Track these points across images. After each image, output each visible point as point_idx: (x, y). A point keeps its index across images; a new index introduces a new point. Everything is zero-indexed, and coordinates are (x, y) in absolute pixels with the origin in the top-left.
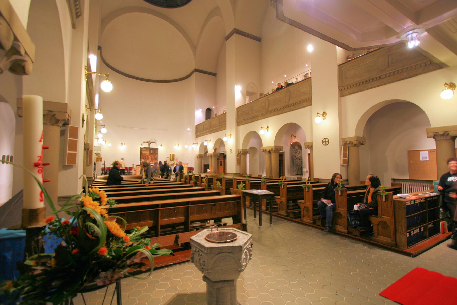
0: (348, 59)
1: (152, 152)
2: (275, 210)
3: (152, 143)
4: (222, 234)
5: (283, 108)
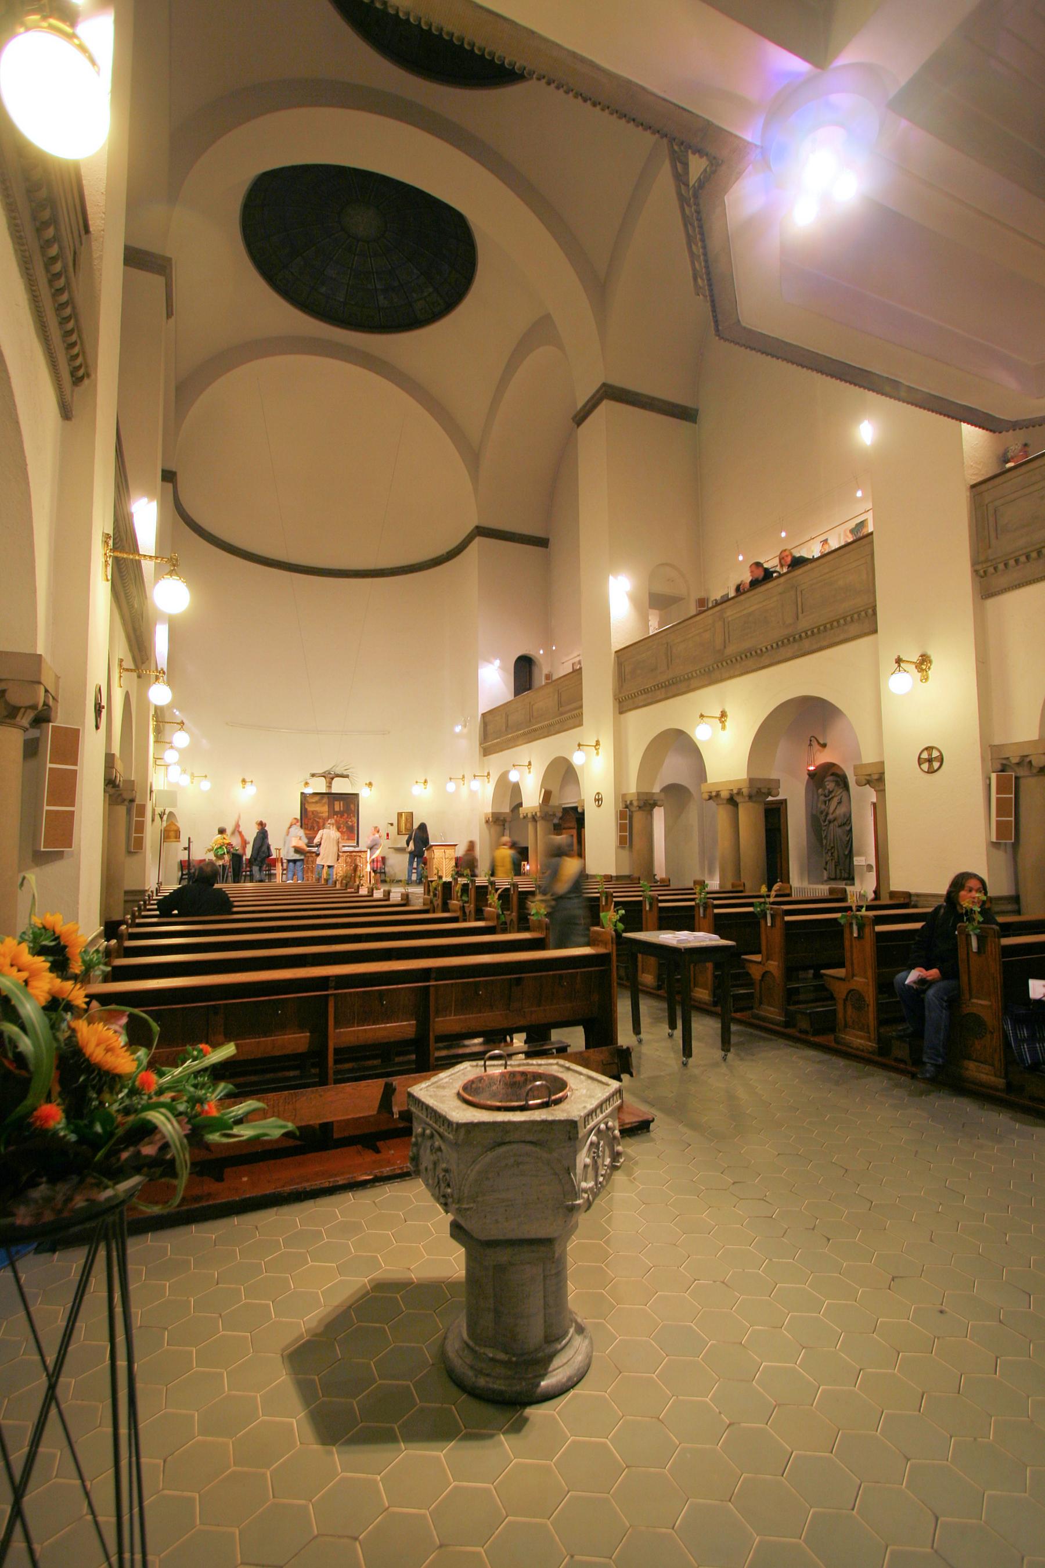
0: (1007, 463)
1: (338, 806)
2: (745, 1003)
3: (338, 776)
4: (519, 1078)
5: (774, 645)
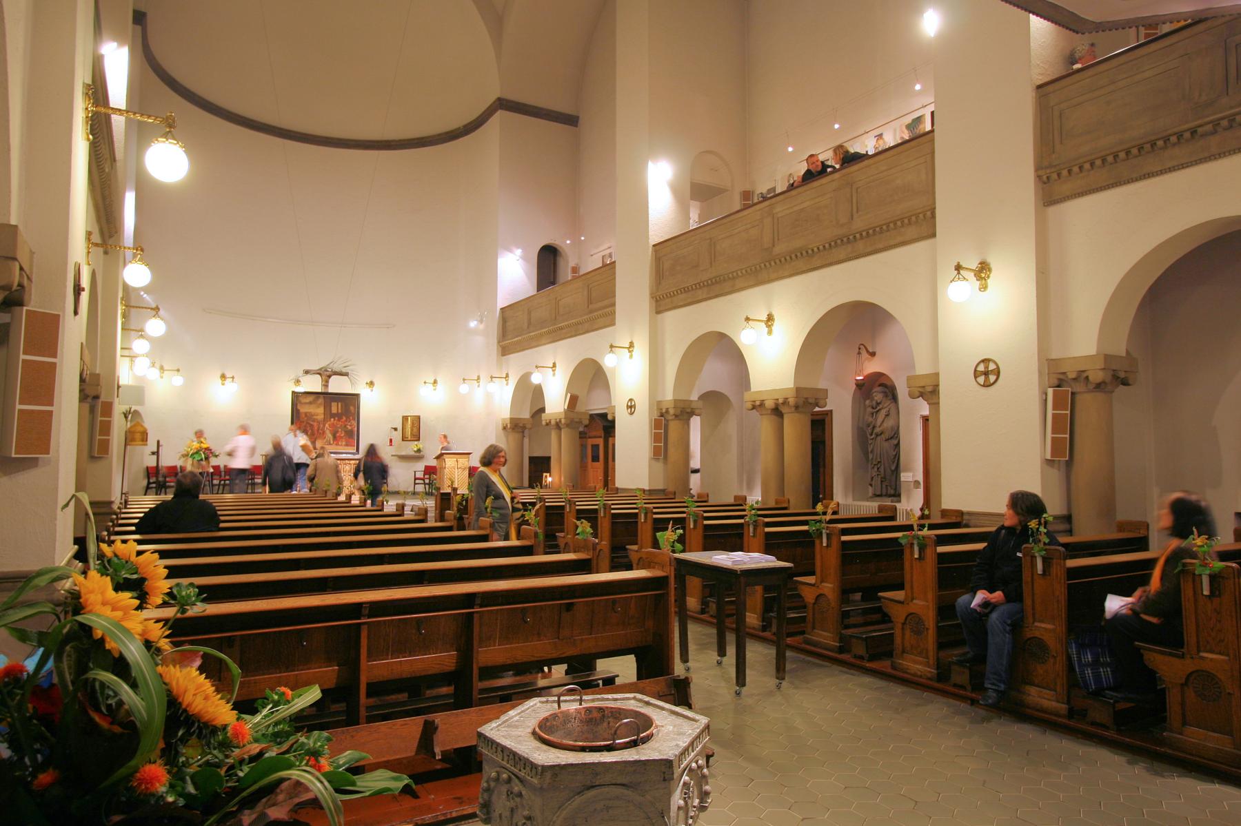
4: (595, 714)
5: (827, 246)
